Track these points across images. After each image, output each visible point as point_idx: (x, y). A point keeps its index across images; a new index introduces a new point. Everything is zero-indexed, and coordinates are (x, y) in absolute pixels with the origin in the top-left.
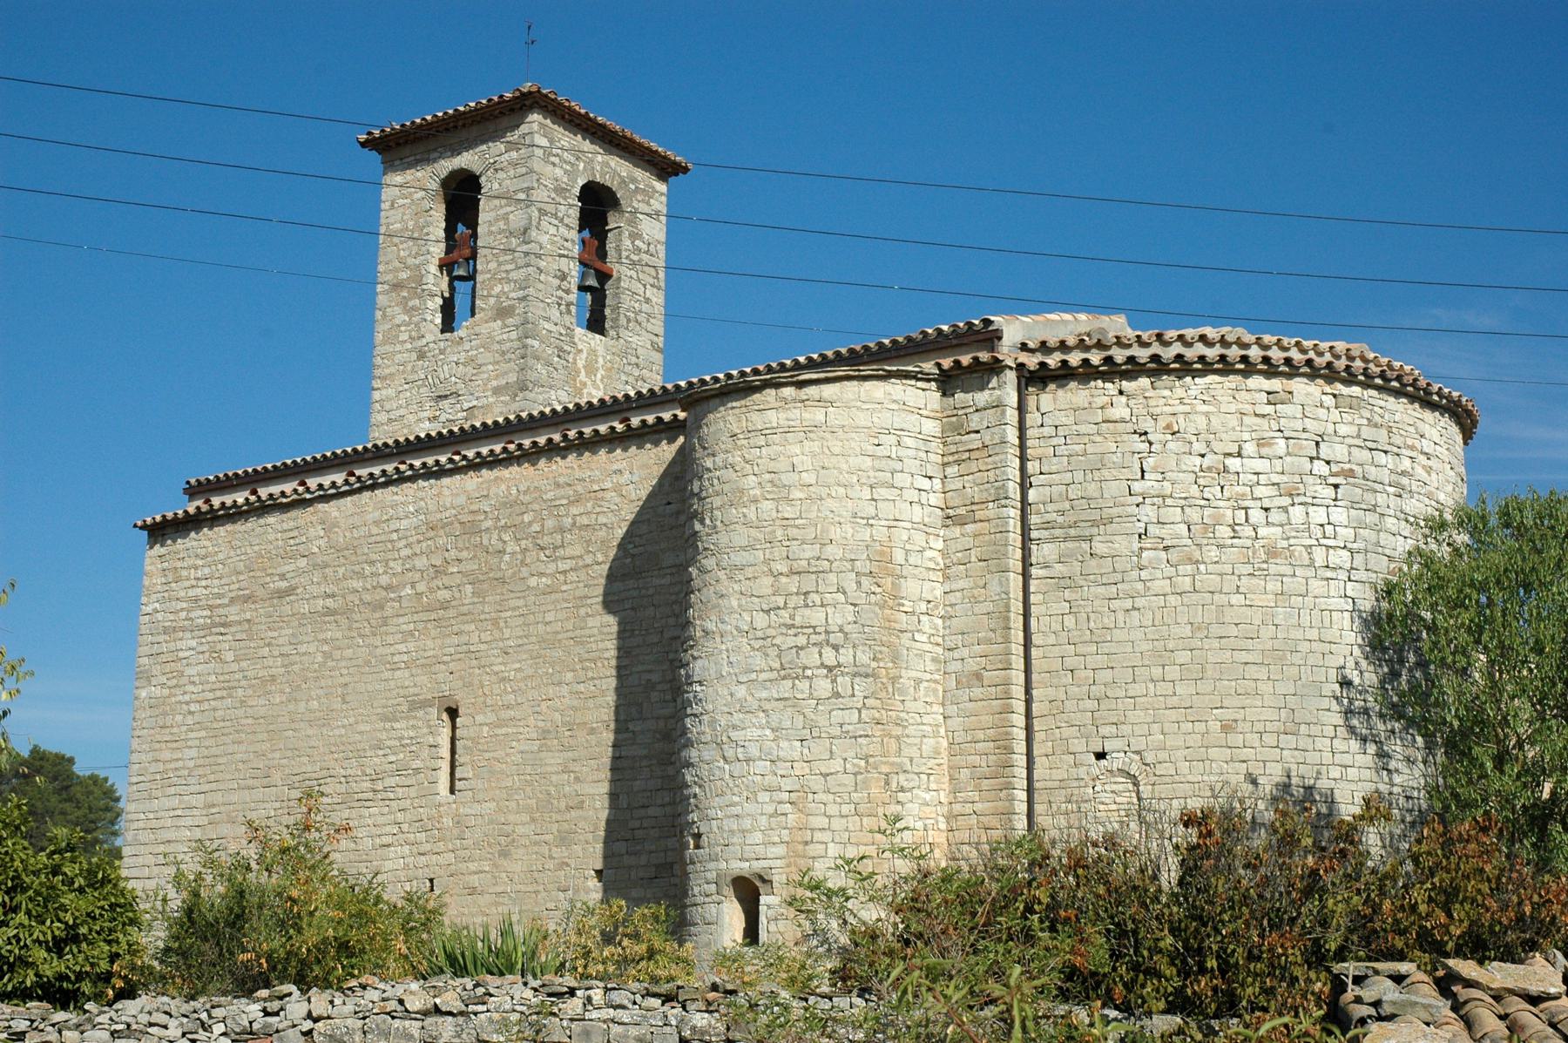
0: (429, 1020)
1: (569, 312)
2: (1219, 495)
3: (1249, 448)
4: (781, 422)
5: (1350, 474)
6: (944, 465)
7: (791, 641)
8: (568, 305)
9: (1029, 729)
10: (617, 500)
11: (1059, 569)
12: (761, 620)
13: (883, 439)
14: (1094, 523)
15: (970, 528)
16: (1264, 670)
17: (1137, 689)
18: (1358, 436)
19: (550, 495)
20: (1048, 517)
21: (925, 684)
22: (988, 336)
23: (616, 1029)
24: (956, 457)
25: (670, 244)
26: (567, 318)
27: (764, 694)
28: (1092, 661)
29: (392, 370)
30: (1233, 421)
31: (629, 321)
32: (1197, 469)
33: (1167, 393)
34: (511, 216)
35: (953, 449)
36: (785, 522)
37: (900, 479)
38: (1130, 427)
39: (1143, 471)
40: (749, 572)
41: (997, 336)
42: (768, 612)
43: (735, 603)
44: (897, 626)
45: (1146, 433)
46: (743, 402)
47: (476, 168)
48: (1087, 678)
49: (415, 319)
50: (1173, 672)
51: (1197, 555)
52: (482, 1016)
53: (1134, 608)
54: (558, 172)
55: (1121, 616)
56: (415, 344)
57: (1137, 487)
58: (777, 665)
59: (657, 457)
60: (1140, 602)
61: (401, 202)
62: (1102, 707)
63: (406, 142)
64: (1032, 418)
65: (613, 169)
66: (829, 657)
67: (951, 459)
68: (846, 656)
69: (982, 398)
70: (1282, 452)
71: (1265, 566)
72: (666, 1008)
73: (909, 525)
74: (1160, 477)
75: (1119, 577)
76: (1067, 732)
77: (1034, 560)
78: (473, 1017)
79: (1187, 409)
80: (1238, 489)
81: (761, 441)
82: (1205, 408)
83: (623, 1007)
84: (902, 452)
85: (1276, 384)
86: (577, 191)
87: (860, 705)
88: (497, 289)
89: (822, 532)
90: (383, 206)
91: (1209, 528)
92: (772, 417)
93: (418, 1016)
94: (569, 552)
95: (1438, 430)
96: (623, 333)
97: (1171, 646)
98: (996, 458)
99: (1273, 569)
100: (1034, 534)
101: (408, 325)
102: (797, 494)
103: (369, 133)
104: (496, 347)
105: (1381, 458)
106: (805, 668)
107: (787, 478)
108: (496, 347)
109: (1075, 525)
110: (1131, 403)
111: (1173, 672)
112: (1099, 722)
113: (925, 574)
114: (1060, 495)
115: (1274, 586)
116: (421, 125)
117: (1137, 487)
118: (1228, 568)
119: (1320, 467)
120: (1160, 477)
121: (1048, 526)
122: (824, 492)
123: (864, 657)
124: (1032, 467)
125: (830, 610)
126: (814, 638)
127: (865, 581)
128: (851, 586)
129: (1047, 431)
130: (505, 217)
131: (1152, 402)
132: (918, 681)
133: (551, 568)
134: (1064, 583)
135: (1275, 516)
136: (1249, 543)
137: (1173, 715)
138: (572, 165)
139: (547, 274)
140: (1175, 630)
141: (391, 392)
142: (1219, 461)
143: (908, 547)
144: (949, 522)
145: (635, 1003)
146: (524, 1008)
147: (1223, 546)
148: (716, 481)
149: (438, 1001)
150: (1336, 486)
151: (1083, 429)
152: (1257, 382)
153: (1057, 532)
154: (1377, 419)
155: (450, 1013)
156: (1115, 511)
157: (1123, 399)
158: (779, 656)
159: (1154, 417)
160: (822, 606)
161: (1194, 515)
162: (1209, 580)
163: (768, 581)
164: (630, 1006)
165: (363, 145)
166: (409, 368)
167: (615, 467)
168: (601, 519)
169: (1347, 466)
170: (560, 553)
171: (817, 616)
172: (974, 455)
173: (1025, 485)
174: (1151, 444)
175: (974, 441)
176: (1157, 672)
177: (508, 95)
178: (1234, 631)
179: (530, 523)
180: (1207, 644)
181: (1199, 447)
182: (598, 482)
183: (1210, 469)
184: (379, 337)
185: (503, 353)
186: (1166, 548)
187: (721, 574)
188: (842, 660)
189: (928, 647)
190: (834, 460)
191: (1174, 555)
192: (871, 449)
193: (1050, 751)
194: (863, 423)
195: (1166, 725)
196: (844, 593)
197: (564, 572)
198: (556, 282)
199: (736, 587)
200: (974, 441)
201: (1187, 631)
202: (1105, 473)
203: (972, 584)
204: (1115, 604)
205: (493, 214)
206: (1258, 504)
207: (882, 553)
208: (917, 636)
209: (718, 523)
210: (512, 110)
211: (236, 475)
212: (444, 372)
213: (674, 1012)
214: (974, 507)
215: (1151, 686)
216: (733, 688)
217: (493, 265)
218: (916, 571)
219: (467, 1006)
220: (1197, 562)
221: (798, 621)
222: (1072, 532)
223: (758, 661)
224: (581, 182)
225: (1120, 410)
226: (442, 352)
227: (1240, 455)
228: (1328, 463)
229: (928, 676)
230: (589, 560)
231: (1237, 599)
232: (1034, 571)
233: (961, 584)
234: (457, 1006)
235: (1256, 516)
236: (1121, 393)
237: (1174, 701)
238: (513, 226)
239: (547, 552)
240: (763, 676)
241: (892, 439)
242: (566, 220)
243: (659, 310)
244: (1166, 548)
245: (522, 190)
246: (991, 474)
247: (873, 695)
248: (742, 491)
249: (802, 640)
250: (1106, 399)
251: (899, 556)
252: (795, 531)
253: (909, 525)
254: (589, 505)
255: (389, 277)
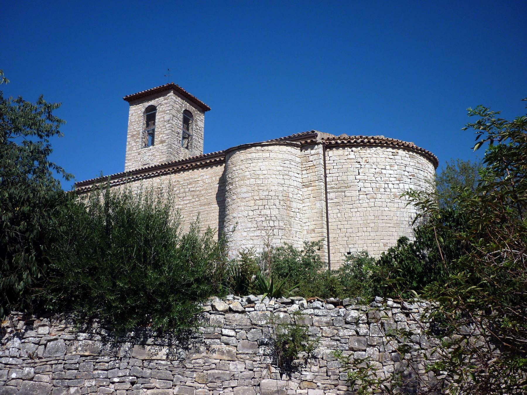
0: (227, 315)
1: (180, 143)
2: (380, 180)
3: (388, 167)
4: (257, 156)
5: (413, 176)
6: (302, 171)
7: (260, 219)
8: (180, 141)
9: (328, 246)
10: (202, 183)
11: (335, 200)
12: (251, 213)
13: (286, 162)
14: (346, 187)
15: (310, 188)
16: (395, 229)
17: (359, 234)
18: (415, 166)
19: (182, 183)
20: (332, 186)
21: (298, 233)
22: (313, 135)
23: (316, 318)
24: (306, 168)
25: (205, 128)
26: (179, 144)
27: (252, 235)
28: (346, 226)
29: (131, 158)
30: (383, 160)
31: (195, 147)
32: (374, 173)
33: (365, 151)
34: (165, 117)
35: (305, 166)
36: (258, 185)
37: (290, 173)
38: (355, 161)
39: (359, 173)
40: (247, 199)
41: (316, 135)
42: (253, 211)
43: (243, 208)
44: (291, 215)
45: (360, 162)
46: (245, 151)
47: (156, 105)
48: (345, 231)
49: (138, 144)
50: (369, 229)
51: (375, 196)
52: (253, 312)
53: (358, 211)
54: (178, 106)
55: (354, 213)
56: (138, 151)
57: (358, 177)
58: (256, 226)
59: (219, 170)
60: (359, 209)
61: (134, 114)
62: (349, 239)
63: (136, 99)
64: (327, 158)
65: (192, 109)
66: (272, 224)
67: (304, 169)
68: (276, 223)
69: (313, 152)
70: (396, 169)
71: (394, 200)
72: (337, 309)
73: (293, 187)
74: (364, 174)
75: (353, 202)
76: (339, 247)
77: (328, 198)
78: (248, 313)
79: (371, 156)
80: (385, 178)
81: (250, 162)
82: (376, 156)
83: (319, 309)
84: (291, 166)
85: (394, 151)
86: (182, 112)
87: (281, 238)
88: (161, 136)
89: (269, 188)
90: (129, 115)
91: (378, 189)
92: (254, 155)
93: (223, 313)
94: (188, 198)
95: (431, 166)
96: (193, 150)
97: (368, 222)
98: (318, 168)
99: (396, 201)
100: (328, 191)
101: (136, 146)
102: (261, 177)
103: (127, 96)
104: (160, 151)
105: (421, 172)
106: (264, 227)
107: (259, 172)
108: (160, 151)
109: (340, 188)
110: (355, 154)
111: (369, 229)
112: (348, 244)
113: (298, 201)
114: (336, 179)
115: (396, 205)
116: (141, 94)
117: (358, 177)
118: (384, 200)
119: (406, 173)
120: (364, 174)
121: (332, 188)
122: (269, 176)
123: (282, 224)
124: (327, 172)
125: (272, 210)
126: (267, 218)
127: (282, 202)
128: (277, 204)
129: (331, 162)
130: (163, 117)
131: (361, 154)
132: (297, 232)
133: (182, 203)
134: (337, 204)
135: (396, 186)
136: (389, 193)
137: (370, 241)
138: (181, 105)
139: (174, 132)
140: (370, 217)
141: (130, 164)
142: (380, 171)
143: (293, 193)
144: (304, 187)
145: (322, 306)
146: (272, 309)
147: (382, 194)
148: (236, 174)
149: (231, 306)
150: (411, 179)
151: (342, 161)
152: (390, 149)
153: (335, 190)
154: (419, 161)
155: (237, 312)
156: (351, 184)
157: (353, 153)
158: (257, 223)
159: (362, 158)
160: (269, 209)
161: (374, 185)
162: (378, 204)
163: (253, 202)
164: (321, 308)
165: (125, 99)
166: (136, 157)
167: (202, 174)
168: (198, 189)
169: (413, 174)
170: (185, 198)
171: (268, 212)
172: (311, 168)
173: (326, 177)
174: (361, 165)
175: (311, 164)
176: (365, 229)
177: (165, 85)
178: (386, 218)
179: (176, 191)
180: (378, 221)
181: (374, 166)
182: (197, 178)
183: (378, 173)
184: (127, 149)
185: (162, 153)
186: (366, 194)
187: (238, 200)
188: (275, 224)
189: (299, 222)
190: (272, 167)
191: (368, 196)
192: (283, 165)
193: (334, 252)
194: (280, 157)
195: (368, 244)
196: (275, 205)
197: (186, 204)
198: (177, 135)
199: (243, 204)
200: (311, 164)
201: (373, 218)
202: (348, 173)
203: (311, 204)
204: (352, 210)
205: (160, 116)
206: (391, 182)
207: (286, 194)
208: (296, 219)
209: (238, 186)
210: (166, 90)
211: (89, 181)
212: (145, 158)
213: (342, 310)
214: (311, 182)
215: (363, 233)
216: (243, 233)
217: (160, 130)
218: (296, 200)
219: (245, 308)
220: (375, 198)
221: (262, 213)
222: (339, 190)
223: (249, 225)
224: (183, 109)
225: (352, 156)
226: (145, 153)
227: (385, 169)
228: (408, 172)
229: (299, 230)
230: (194, 200)
231: (386, 209)
232: (329, 201)
233: (308, 204)
234: (240, 308)
235: (391, 186)
236: (352, 151)
237: (370, 237)
238: (165, 119)
239: (181, 198)
240: (252, 229)
241: (289, 162)
242: (180, 119)
243: (202, 146)
244: (366, 194)
245: (168, 110)
246: (316, 173)
247: (284, 235)
248: (245, 176)
249: (263, 219)
250: (348, 153)
251: (291, 195)
252: (261, 187)
253: (293, 187)
254: (194, 185)
255: (131, 134)
